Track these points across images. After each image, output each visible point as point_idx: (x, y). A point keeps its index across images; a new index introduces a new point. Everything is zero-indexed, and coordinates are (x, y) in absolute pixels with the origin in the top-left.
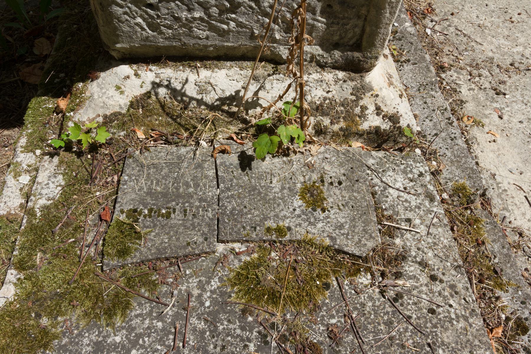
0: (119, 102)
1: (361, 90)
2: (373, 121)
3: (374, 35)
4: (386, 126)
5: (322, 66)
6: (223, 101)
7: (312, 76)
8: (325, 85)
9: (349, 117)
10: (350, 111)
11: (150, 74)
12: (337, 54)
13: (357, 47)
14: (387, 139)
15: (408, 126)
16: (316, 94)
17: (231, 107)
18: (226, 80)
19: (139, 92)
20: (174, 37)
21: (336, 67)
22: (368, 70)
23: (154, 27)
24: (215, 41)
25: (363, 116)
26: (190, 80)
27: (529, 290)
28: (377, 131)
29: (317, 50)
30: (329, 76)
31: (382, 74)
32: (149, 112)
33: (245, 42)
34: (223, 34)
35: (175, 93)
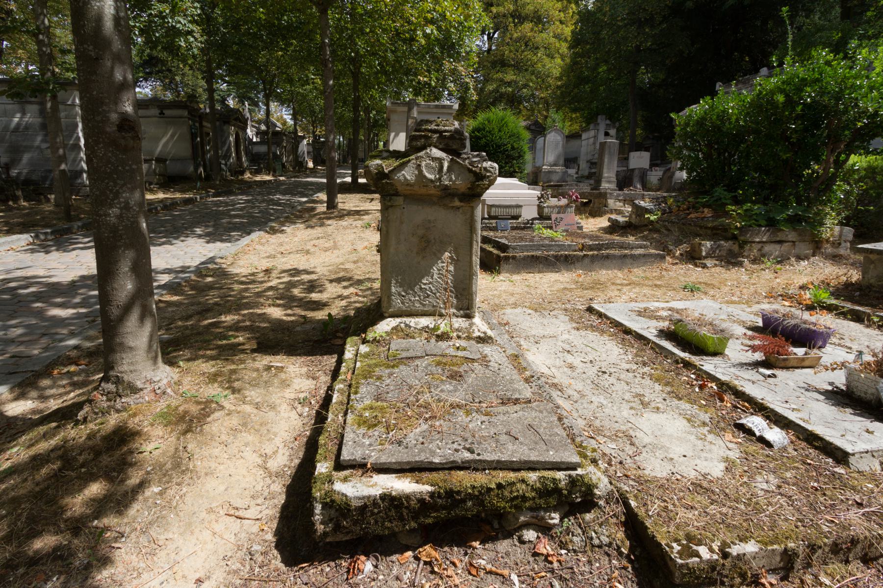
0: (388, 328)
1: (471, 325)
2: (477, 334)
3: (472, 304)
4: (482, 335)
5: (457, 317)
6: (423, 328)
7: (454, 320)
8: (459, 323)
9: (469, 332)
10: (469, 331)
11: (398, 320)
12: (462, 312)
13: (468, 309)
14: (484, 340)
15: (282, 232)
16: (456, 326)
17: (425, 329)
18: (424, 321)
19: (395, 325)
20: (409, 307)
21: (462, 317)
22: (473, 317)
23: (403, 303)
24: (422, 308)
25: (473, 332)
26: (412, 321)
27: (608, 587)
28: (479, 337)
29: (455, 311)
30: (460, 320)
31: (477, 320)
32: (398, 331)
33: (431, 308)
34: (424, 305)
35: (406, 325)
